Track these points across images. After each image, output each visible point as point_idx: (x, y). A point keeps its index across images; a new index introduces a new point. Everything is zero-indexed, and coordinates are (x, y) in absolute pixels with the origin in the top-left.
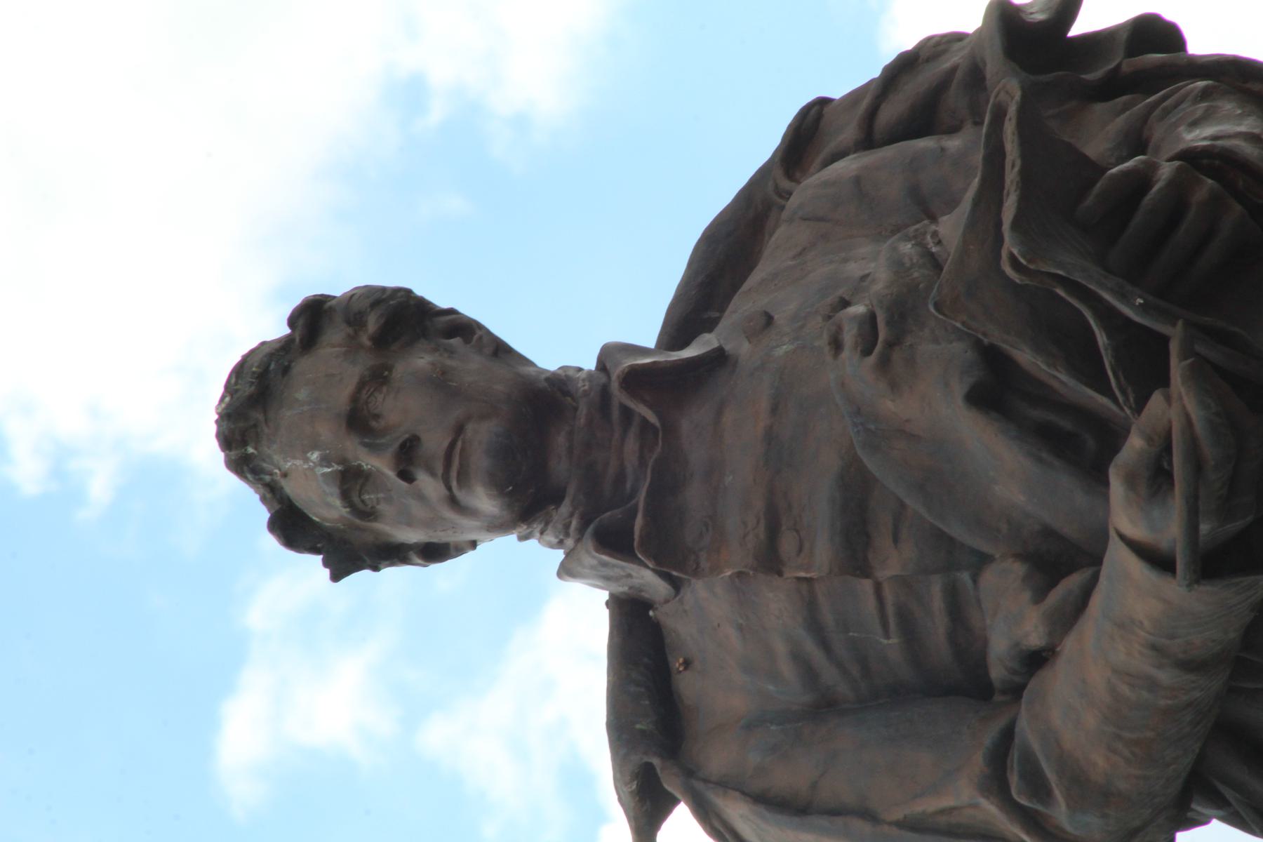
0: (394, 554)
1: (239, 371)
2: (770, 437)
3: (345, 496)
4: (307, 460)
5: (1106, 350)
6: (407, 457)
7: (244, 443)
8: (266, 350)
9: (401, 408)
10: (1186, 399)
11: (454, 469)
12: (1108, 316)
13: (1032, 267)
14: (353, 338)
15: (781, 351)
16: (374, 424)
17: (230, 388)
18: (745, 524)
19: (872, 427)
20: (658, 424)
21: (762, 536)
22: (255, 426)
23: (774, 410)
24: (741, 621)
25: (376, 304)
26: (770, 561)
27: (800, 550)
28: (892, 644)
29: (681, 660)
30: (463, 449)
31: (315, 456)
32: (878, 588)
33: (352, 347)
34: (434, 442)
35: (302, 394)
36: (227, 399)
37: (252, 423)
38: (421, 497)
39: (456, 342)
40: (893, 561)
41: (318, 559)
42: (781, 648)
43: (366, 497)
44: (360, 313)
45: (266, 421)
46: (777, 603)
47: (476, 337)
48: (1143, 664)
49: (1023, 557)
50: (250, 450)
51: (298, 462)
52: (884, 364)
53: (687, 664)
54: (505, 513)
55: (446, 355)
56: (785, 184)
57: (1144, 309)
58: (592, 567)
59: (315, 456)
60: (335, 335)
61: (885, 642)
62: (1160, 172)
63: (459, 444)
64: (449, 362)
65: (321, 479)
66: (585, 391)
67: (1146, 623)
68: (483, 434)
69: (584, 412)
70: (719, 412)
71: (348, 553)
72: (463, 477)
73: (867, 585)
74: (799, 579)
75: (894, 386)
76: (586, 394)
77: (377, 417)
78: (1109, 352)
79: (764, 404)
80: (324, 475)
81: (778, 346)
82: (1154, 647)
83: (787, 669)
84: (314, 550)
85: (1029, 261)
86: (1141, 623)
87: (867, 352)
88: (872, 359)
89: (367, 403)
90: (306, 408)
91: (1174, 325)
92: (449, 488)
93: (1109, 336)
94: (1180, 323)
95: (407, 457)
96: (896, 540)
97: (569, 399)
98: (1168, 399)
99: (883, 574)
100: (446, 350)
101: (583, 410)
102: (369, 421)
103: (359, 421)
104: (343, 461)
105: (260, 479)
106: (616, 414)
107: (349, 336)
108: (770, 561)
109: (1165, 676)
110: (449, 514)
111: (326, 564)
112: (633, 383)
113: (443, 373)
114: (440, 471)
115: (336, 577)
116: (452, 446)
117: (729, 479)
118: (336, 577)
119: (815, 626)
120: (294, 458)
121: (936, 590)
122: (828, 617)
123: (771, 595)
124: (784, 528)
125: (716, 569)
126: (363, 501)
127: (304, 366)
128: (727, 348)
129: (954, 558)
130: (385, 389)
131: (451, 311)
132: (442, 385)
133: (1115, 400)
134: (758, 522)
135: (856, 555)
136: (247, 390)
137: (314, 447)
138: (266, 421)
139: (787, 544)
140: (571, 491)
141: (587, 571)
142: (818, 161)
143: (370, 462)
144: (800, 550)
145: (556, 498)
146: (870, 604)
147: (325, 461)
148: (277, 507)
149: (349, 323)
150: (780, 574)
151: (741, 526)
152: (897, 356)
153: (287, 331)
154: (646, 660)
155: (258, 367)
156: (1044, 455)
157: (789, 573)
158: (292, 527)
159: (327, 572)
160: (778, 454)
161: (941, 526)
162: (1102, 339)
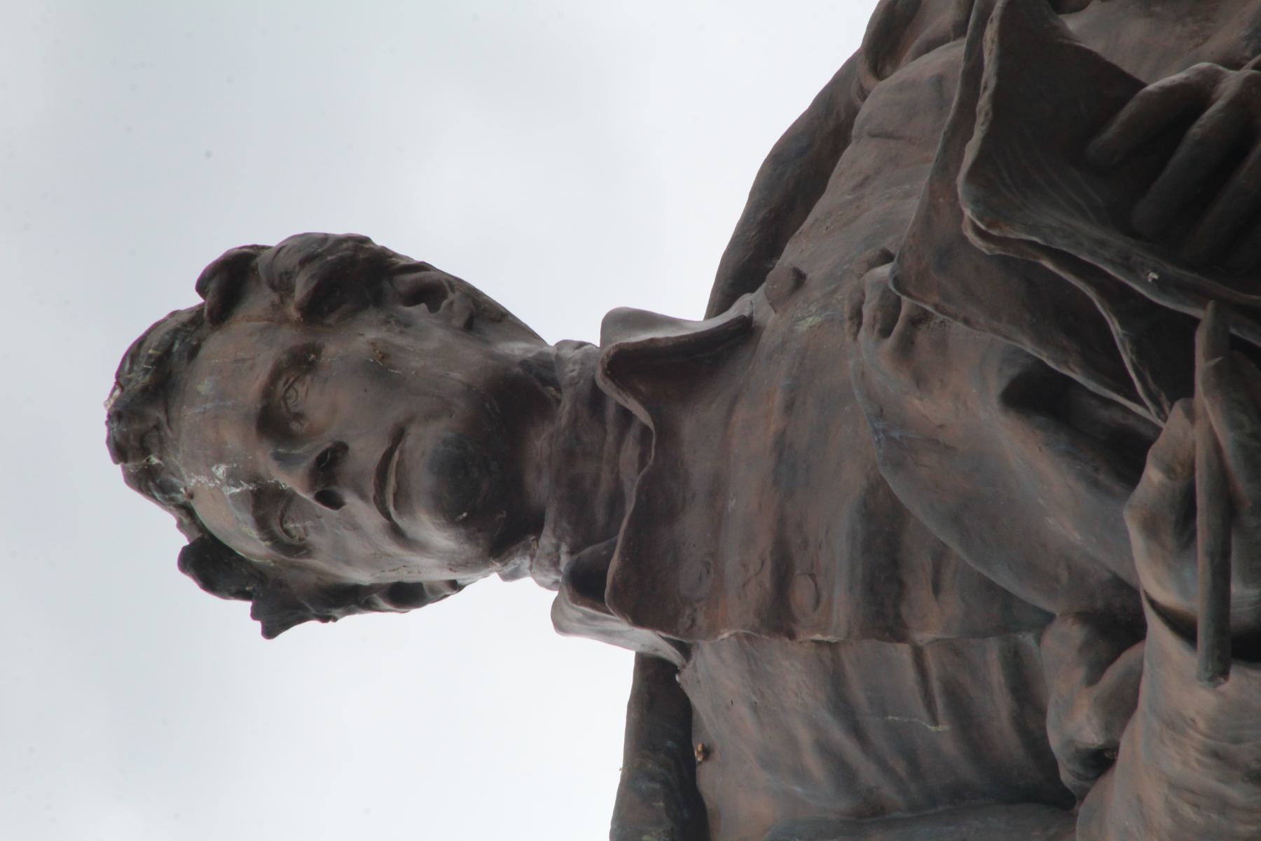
0: (339, 599)
1: (134, 354)
2: (782, 446)
3: (262, 524)
4: (212, 477)
5: (1123, 342)
6: (328, 475)
7: (145, 451)
8: (173, 324)
9: (330, 405)
10: (1210, 413)
11: (388, 489)
12: (1119, 296)
13: (995, 232)
14: (276, 307)
15: (803, 327)
16: (295, 426)
17: (121, 380)
18: (745, 566)
19: (896, 435)
20: (651, 426)
21: (768, 585)
22: (157, 427)
23: (789, 408)
24: (754, 698)
25: (306, 261)
26: (778, 618)
27: (818, 602)
28: (942, 732)
29: (700, 748)
30: (398, 465)
31: (221, 471)
32: (918, 654)
33: (276, 318)
34: (366, 452)
35: (205, 386)
36: (117, 393)
37: (151, 424)
38: (355, 527)
39: (420, 310)
40: (934, 619)
41: (246, 606)
42: (804, 736)
43: (290, 526)
44: (287, 273)
45: (168, 421)
46: (793, 672)
47: (445, 303)
48: (1204, 777)
49: (1084, 617)
50: (155, 460)
51: (203, 479)
52: (906, 348)
53: (707, 752)
54: (466, 547)
55: (397, 329)
56: (869, 81)
57: (1162, 285)
58: (580, 621)
59: (221, 471)
60: (258, 302)
61: (933, 728)
62: (1222, 86)
63: (397, 454)
64: (399, 341)
65: (229, 501)
66: (573, 378)
67: (1201, 725)
68: (426, 441)
69: (568, 407)
70: (730, 412)
71: (287, 596)
72: (402, 499)
73: (902, 652)
74: (818, 642)
75: (920, 381)
76: (573, 382)
77: (299, 416)
78: (1128, 346)
79: (778, 400)
80: (232, 496)
81: (804, 318)
82: (1215, 754)
83: (814, 764)
84: (242, 595)
85: (989, 225)
86: (1193, 721)
87: (886, 332)
88: (890, 342)
89: (285, 398)
90: (209, 405)
91: (1204, 307)
92: (387, 515)
93: (1123, 324)
94: (1211, 305)
95: (328, 475)
96: (937, 589)
97: (552, 389)
98: (1190, 414)
99: (923, 637)
100: (398, 322)
101: (566, 406)
102: (326, 420)
103: (273, 423)
104: (254, 478)
105: (172, 499)
106: (611, 412)
107: (273, 305)
108: (778, 618)
109: (1237, 793)
110: (393, 548)
111: (255, 615)
112: (654, 366)
113: (384, 357)
114: (371, 493)
115: (270, 632)
116: (387, 457)
117: (732, 504)
118: (270, 632)
119: (844, 709)
120: (198, 473)
121: (992, 655)
122: (858, 694)
123: (786, 663)
124: (798, 572)
125: (713, 631)
126: (286, 532)
127: (219, 347)
128: (756, 317)
129: (1007, 617)
130: (308, 377)
131: (422, 267)
132: (381, 370)
133: (1147, 408)
134: (763, 563)
135: (884, 614)
136: (141, 379)
137: (220, 458)
138: (168, 421)
139: (802, 593)
140: (550, 515)
141: (576, 625)
142: (909, 53)
143: (291, 481)
144: (818, 602)
145: (536, 527)
146: (910, 674)
147: (233, 478)
148: (197, 535)
149: (274, 288)
150: (791, 635)
151: (744, 571)
152: (923, 337)
153: (197, 300)
154: (669, 743)
155: (156, 349)
156: (1102, 477)
157: (809, 636)
158: (209, 563)
159: (258, 625)
160: (790, 467)
161: (985, 573)
162: (1115, 328)
